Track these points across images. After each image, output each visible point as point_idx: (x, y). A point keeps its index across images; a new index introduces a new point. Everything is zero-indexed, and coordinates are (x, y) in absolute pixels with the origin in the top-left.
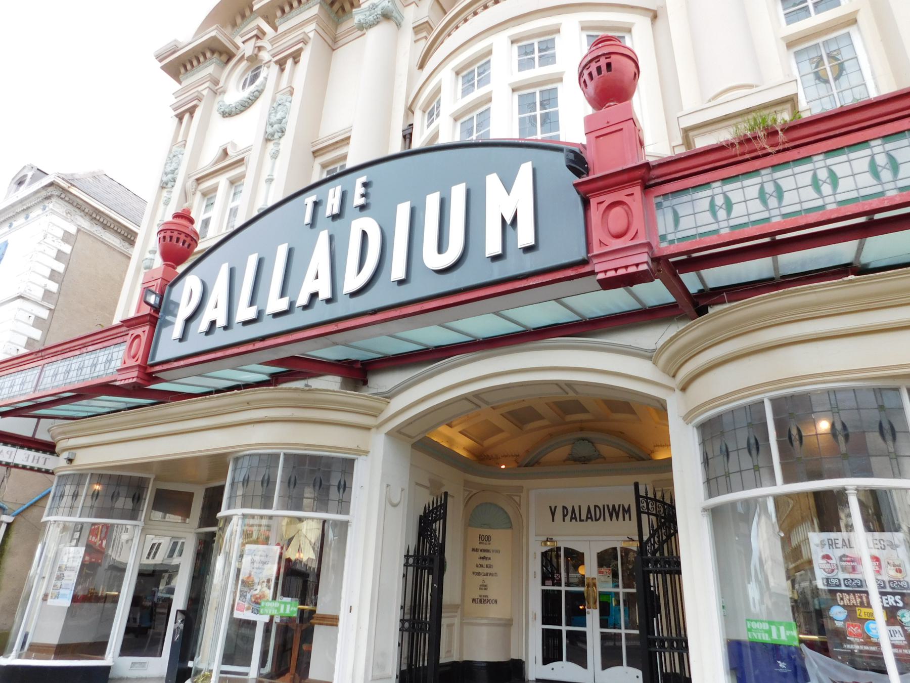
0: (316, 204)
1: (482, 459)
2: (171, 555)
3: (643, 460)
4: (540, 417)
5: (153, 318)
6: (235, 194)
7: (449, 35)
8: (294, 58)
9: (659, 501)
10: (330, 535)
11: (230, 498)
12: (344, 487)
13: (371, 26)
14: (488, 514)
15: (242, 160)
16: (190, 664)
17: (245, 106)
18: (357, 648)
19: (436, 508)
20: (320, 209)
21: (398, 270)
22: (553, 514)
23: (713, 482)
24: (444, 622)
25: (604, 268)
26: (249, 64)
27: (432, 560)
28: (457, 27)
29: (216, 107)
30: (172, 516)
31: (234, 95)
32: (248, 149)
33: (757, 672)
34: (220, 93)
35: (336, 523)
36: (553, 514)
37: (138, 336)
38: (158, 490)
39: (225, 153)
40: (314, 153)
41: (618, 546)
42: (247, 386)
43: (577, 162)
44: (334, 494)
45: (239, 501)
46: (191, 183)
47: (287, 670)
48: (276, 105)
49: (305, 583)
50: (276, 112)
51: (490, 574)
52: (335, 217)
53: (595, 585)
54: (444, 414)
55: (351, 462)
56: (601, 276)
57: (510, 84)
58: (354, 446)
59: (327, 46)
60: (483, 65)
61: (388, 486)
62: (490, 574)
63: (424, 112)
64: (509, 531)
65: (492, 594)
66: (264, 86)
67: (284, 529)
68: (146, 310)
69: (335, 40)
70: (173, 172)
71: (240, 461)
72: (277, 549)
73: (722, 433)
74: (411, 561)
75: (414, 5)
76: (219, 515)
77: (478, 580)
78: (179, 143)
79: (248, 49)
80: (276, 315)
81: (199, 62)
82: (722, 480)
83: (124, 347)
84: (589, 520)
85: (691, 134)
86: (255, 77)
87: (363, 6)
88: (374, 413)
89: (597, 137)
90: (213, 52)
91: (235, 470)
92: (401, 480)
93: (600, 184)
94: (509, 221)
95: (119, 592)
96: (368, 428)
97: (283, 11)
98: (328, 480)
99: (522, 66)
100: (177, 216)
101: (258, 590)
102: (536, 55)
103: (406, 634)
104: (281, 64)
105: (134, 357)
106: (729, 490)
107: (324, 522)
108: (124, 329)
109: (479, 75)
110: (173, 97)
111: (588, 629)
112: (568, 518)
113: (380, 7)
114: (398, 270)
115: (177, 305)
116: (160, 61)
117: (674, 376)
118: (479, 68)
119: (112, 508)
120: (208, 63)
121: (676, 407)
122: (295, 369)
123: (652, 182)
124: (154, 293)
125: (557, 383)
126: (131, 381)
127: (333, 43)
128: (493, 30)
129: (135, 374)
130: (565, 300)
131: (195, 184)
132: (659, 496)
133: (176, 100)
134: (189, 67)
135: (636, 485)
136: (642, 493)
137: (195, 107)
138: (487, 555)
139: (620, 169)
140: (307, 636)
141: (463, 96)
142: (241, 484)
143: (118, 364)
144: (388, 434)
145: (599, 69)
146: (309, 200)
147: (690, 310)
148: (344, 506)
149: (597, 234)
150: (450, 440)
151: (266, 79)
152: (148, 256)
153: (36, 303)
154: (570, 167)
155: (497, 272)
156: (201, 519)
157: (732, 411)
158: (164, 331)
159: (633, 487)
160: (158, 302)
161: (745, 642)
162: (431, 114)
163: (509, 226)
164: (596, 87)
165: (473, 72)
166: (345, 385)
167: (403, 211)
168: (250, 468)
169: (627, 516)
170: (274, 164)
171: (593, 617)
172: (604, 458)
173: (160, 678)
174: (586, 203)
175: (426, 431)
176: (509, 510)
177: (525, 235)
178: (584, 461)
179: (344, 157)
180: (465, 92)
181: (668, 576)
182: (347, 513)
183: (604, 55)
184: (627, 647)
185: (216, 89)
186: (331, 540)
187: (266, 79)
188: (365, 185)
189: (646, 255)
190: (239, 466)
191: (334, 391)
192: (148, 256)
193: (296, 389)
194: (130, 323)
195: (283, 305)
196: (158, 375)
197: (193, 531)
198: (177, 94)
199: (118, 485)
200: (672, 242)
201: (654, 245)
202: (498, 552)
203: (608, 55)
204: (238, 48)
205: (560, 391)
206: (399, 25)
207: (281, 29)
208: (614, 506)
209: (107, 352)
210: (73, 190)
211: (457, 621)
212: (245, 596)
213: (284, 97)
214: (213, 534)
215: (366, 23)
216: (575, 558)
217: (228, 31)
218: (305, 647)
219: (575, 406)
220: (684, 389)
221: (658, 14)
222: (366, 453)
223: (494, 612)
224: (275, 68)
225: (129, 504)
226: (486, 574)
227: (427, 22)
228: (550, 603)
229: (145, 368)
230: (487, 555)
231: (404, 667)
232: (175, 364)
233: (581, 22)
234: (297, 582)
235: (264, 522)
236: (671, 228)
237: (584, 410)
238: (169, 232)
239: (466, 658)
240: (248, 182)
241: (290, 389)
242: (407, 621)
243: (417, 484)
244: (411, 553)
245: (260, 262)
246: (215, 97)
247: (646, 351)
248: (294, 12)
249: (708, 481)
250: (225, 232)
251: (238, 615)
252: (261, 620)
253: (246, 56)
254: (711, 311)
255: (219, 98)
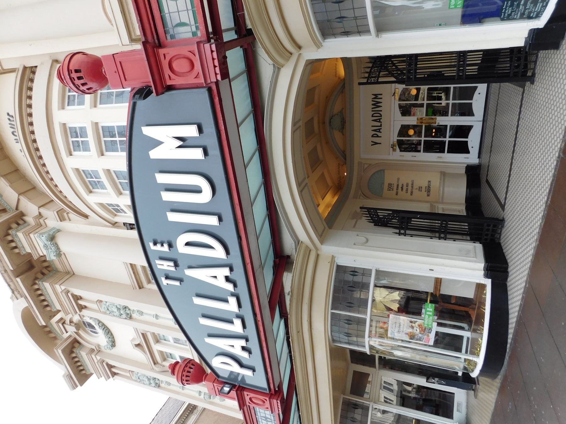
0: (167, 278)
1: (340, 187)
2: (392, 391)
3: (344, 84)
4: (315, 149)
5: (239, 388)
6: (165, 340)
7: (66, 197)
8: (78, 299)
9: (371, 70)
10: (384, 282)
11: (358, 345)
12: (354, 272)
13: (58, 248)
14: (375, 182)
15: (143, 334)
16: (460, 374)
17: (108, 332)
18: (456, 267)
19: (370, 214)
20: (171, 275)
21: (212, 221)
22: (376, 143)
23: (360, 29)
24: (440, 212)
25: (214, 75)
26: (81, 329)
27: (403, 218)
28: (61, 192)
29: (108, 351)
30: (367, 388)
31: (101, 339)
32: (136, 330)
33: (480, 4)
34: (99, 348)
35: (377, 278)
36: (376, 143)
37: (250, 399)
38: (351, 393)
39: (138, 345)
40: (140, 288)
41: (397, 103)
42: (287, 333)
43: (143, 93)
44: (358, 279)
45: (360, 340)
46: (156, 368)
47: (467, 312)
48: (108, 312)
49: (413, 299)
50: (113, 312)
51: (412, 184)
52: (176, 265)
53: (421, 119)
54: (311, 208)
55: (339, 267)
56: (219, 77)
57: (99, 157)
58: (329, 265)
59: (71, 278)
60: (86, 175)
61: (355, 244)
62: (412, 184)
63: (116, 215)
64: (386, 171)
65: (425, 184)
66: (96, 319)
67: (379, 311)
68: (233, 393)
69: (68, 273)
70: (149, 379)
71: (335, 338)
72: (392, 316)
73: (329, 21)
74: (402, 231)
75: (45, 221)
76: (368, 353)
77: (416, 192)
78: (131, 376)
79: (71, 329)
80: (240, 306)
81: (78, 361)
82: (359, 22)
83: (257, 409)
84: (381, 131)
85: (134, 37)
87: (45, 253)
88: (308, 251)
89: (126, 80)
90: (72, 352)
91: (340, 342)
92: (352, 236)
93: (157, 77)
94: (180, 143)
95: (413, 418)
96: (318, 256)
97: (47, 306)
98: (349, 282)
99: (87, 149)
100: (173, 373)
101: (417, 331)
102: (79, 139)
103: (448, 236)
104: (81, 308)
105: (264, 402)
106: (365, 17)
107: (376, 286)
108: (245, 408)
109: (92, 178)
110: (101, 379)
111: (449, 124)
112: (379, 134)
113: (46, 242)
114: (212, 221)
115: (232, 373)
116: (77, 386)
117: (291, 54)
118: (87, 178)
119: (361, 422)
121: (312, 54)
122: (277, 299)
123: (156, 41)
124: (222, 388)
125: (293, 132)
126: (279, 404)
127: (69, 274)
128: (63, 168)
129: (275, 401)
130: (239, 121)
131: (157, 365)
132: (368, 70)
133: (103, 377)
134: (81, 368)
135: (360, 84)
136: (365, 81)
137: (108, 365)
138: (400, 186)
139: (146, 63)
140: (447, 298)
141: (106, 189)
142: (350, 338)
143: (268, 413)
144: (322, 243)
145: (79, 78)
146: (164, 282)
147: (249, 39)
148: (366, 272)
149: (190, 80)
150: (327, 206)
151: (91, 318)
152: (202, 396)
154: (145, 98)
155: (215, 152)
156: (370, 366)
157: (315, 13)
158: (248, 381)
159: (361, 86)
160: (228, 386)
161: (463, 11)
162: (118, 211)
163: (184, 143)
164: (92, 81)
165: (90, 181)
166: (289, 270)
167: (173, 217)
168: (339, 332)
169: (379, 96)
170: (146, 314)
171: (441, 120)
172: (343, 109)
173: (468, 395)
174: (170, 88)
175: (321, 218)
176: (374, 170)
177: (191, 131)
178: (344, 122)
179: (143, 267)
180: (103, 187)
181: (418, 71)
182: (371, 270)
183: (69, 74)
184: (459, 100)
186: (386, 280)
187: (91, 318)
188: (155, 244)
189: (205, 45)
190: (338, 339)
191: (293, 276)
192: (202, 396)
193: (291, 301)
194: (242, 404)
195: (233, 301)
196: (276, 385)
197: (377, 371)
198: (99, 377)
199: (346, 418)
200: (197, 28)
201: (199, 40)
202: (398, 179)
203: (69, 72)
204: (70, 336)
205: (298, 131)
206: (59, 231)
207: (59, 308)
208: (373, 105)
209: (260, 420)
211: (441, 206)
212: (420, 338)
213: (103, 306)
214: (380, 358)
215: (56, 251)
216: (404, 130)
217: (59, 342)
218: (453, 302)
219: (309, 124)
220: (300, 47)
221: (55, 58)
222: (333, 257)
223: (436, 183)
224: (84, 312)
225: (359, 411)
226: (412, 187)
227: (57, 212)
228: (430, 147)
229: (272, 394)
230: (400, 186)
231: (468, 238)
232: (270, 374)
233: (59, 109)
234: (413, 304)
235: (374, 324)
236: (187, 29)
237: (312, 120)
238: (184, 378)
239: (464, 201)
240: (157, 331)
241: (290, 305)
242: (440, 235)
243: (354, 226)
244: (397, 231)
245: (205, 316)
246: (102, 352)
247: (274, 72)
248: (48, 298)
249: (359, 33)
250: (189, 346)
251: (431, 343)
252: (435, 328)
253: (76, 331)
254: (249, 26)
255: (103, 349)
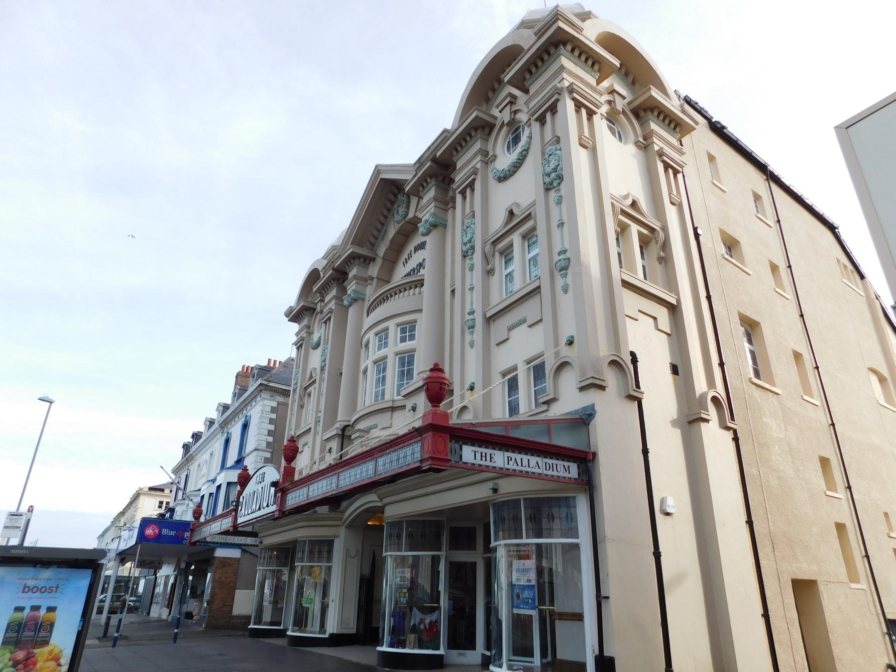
15: (530, 214)
17: (516, 166)
29: (491, 176)
31: (504, 160)
32: (533, 204)
39: (511, 213)
46: (488, 247)
70: (470, 241)
79: (506, 116)
81: (462, 146)
86: (516, 140)
104: (542, 120)
120: (474, 139)
137: (474, 180)
151: (530, 137)
153: (263, 450)
185: (488, 158)
204: (495, 118)
210: (271, 384)
213: (553, 147)
224: (536, 126)
240: (541, 231)
246: (487, 167)
253: (505, 122)
255: (491, 167)
